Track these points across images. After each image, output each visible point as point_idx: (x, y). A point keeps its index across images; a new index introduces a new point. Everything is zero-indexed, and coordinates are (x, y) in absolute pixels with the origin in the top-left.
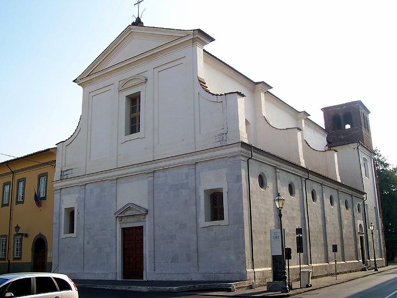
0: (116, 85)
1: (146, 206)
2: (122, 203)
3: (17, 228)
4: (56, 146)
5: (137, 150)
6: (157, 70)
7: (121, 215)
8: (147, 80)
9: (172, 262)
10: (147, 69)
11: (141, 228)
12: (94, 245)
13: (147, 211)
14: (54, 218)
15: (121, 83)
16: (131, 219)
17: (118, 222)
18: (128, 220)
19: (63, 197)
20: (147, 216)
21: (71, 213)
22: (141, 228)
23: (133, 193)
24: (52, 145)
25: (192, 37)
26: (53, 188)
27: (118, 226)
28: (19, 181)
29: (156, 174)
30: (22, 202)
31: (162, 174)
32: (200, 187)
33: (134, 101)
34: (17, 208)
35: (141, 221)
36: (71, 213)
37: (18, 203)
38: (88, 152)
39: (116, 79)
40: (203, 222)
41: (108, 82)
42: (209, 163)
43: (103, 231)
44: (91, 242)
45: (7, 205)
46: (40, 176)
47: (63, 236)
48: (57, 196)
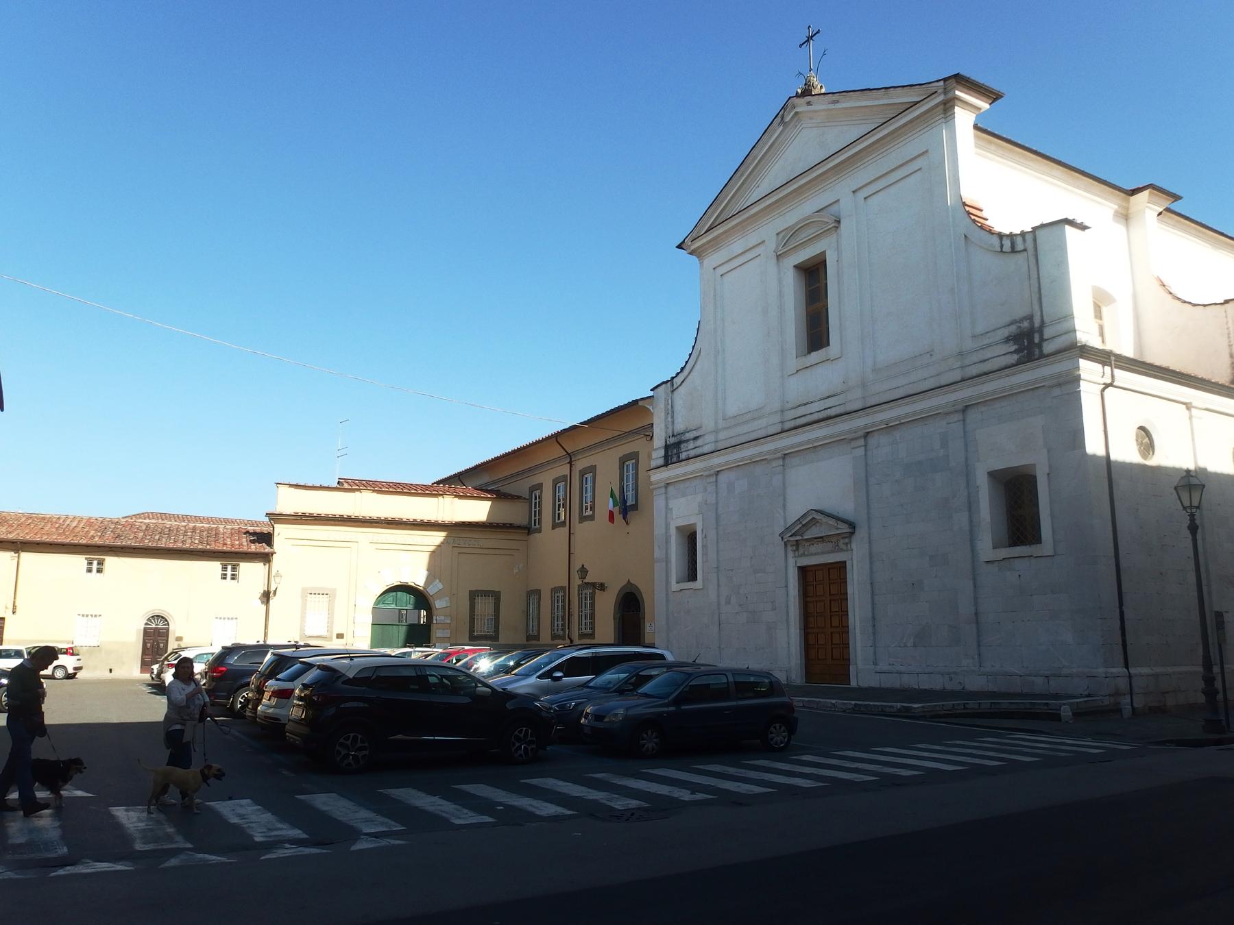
0: (771, 245)
1: (846, 507)
2: (796, 509)
3: (583, 571)
4: (651, 394)
5: (824, 378)
8: (839, 222)
9: (915, 646)
10: (840, 192)
11: (842, 566)
13: (852, 525)
14: (656, 548)
17: (791, 554)
18: (813, 549)
21: (690, 538)
22: (842, 566)
23: (821, 485)
25: (941, 98)
27: (791, 561)
28: (583, 473)
29: (872, 441)
31: (884, 439)
33: (813, 275)
34: (581, 529)
35: (842, 550)
36: (690, 538)
37: (583, 519)
39: (768, 232)
41: (752, 238)
44: (733, 600)
45: (564, 523)
46: (623, 461)
47: (674, 586)
48: (659, 502)
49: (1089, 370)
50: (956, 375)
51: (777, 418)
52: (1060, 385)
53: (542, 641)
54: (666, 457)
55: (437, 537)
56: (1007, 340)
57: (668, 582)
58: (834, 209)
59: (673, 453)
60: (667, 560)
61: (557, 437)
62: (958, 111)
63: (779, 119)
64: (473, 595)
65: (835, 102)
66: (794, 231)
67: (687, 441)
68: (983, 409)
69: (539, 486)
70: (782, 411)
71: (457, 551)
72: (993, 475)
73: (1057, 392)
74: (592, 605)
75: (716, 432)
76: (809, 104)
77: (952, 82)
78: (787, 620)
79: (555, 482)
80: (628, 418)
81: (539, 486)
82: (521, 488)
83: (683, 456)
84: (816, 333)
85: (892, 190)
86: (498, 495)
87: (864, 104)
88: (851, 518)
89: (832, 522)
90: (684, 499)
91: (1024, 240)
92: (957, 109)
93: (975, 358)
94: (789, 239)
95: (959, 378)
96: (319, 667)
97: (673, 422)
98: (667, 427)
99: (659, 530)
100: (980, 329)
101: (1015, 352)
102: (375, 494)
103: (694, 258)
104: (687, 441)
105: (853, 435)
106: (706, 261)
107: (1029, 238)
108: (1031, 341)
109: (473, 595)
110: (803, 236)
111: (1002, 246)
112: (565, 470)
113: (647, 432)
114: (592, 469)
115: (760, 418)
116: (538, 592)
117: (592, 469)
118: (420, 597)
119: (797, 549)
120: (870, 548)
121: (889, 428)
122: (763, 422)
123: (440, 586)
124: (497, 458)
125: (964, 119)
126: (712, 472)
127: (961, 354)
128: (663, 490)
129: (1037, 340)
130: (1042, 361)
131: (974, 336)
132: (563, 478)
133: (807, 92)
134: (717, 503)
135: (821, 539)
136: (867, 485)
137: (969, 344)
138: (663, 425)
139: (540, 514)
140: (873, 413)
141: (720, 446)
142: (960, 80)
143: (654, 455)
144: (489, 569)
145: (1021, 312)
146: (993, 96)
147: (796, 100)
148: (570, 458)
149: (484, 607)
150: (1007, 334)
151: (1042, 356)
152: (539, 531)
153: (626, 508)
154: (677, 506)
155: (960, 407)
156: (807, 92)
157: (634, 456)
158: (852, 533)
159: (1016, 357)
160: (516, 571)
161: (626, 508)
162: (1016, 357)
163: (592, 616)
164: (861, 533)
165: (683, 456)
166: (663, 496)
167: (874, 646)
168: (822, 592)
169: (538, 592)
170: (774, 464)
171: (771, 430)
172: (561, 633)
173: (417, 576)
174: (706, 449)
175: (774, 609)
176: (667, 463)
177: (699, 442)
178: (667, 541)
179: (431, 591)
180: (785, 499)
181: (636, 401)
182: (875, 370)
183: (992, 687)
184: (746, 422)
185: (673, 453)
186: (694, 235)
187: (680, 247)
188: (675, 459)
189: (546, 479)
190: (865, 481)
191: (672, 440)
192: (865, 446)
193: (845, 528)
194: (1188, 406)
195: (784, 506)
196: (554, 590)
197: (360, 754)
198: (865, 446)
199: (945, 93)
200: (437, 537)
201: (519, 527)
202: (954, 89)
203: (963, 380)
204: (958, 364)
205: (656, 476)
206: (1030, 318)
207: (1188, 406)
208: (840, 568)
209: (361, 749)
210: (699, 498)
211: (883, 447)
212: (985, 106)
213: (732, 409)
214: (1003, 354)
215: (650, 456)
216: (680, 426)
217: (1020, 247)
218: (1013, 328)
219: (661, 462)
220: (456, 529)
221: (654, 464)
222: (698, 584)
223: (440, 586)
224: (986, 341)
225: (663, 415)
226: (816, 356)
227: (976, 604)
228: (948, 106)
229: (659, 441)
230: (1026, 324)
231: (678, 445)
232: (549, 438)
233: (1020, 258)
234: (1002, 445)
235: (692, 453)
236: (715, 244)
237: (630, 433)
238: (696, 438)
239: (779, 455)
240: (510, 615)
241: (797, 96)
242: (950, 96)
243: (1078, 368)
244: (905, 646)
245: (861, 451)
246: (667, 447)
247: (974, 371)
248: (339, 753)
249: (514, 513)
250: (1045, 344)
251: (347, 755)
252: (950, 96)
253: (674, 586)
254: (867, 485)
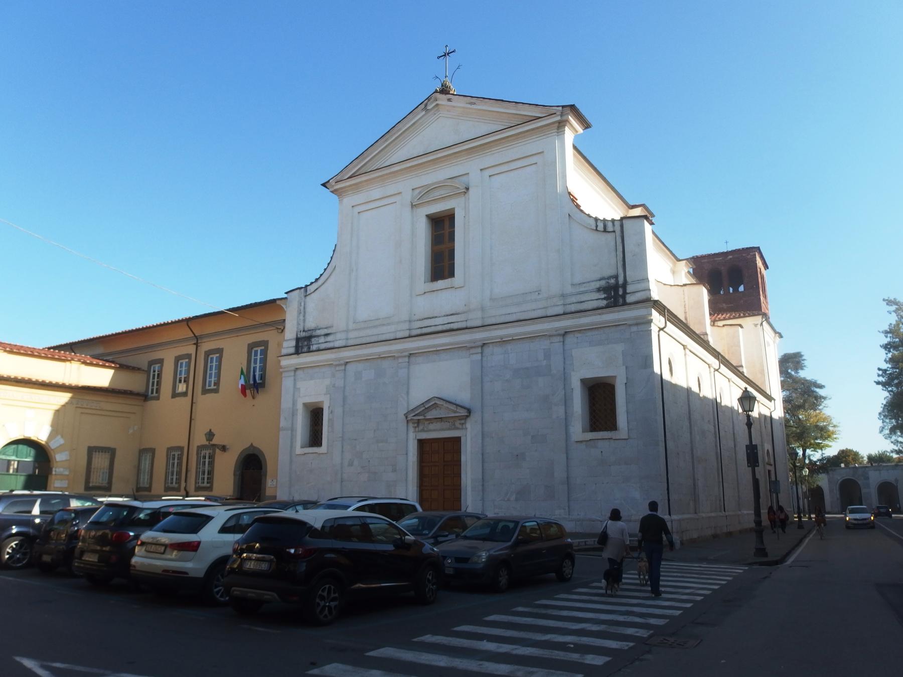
0: (408, 197)
1: (464, 397)
2: (419, 395)
3: (210, 435)
4: (286, 296)
5: (445, 300)
6: (487, 173)
7: (418, 416)
8: (467, 189)
9: (517, 500)
10: (471, 168)
11: (458, 440)
12: (362, 467)
13: (469, 411)
14: (282, 419)
15: (417, 191)
16: (438, 425)
17: (411, 430)
18: (431, 426)
19: (300, 384)
20: (469, 420)
21: (315, 415)
22: (458, 440)
23: (442, 378)
24: (277, 293)
25: (558, 118)
26: (281, 367)
27: (412, 435)
28: (208, 354)
29: (487, 350)
30: (216, 391)
31: (497, 350)
32: (573, 373)
33: (442, 226)
34: (205, 402)
35: (458, 429)
36: (315, 415)
37: (205, 391)
38: (103, 413)
39: (406, 186)
40: (577, 428)
41: (391, 189)
42: (589, 333)
43: (380, 445)
44: (356, 463)
45: (185, 394)
46: (251, 347)
47: (299, 450)
48: (287, 383)
49: (657, 319)
50: (560, 310)
51: (406, 326)
52: (637, 324)
53: (153, 492)
54: (297, 347)
55: (64, 397)
56: (599, 290)
57: (292, 446)
58: (464, 179)
59: (303, 344)
60: (293, 429)
61: (188, 321)
62: (567, 129)
63: (423, 106)
64: (91, 451)
65: (471, 103)
66: (428, 190)
67: (318, 336)
68: (579, 335)
69: (161, 361)
70: (410, 321)
71: (80, 410)
72: (584, 381)
73: (634, 329)
74: (212, 464)
75: (347, 331)
76: (449, 100)
77: (568, 110)
78: (406, 480)
79: (178, 359)
80: (264, 313)
81: (161, 361)
82: (142, 360)
83: (314, 347)
84: (442, 265)
85: (512, 174)
86: (121, 367)
87: (484, 108)
88: (467, 405)
89: (453, 407)
90: (312, 382)
91: (614, 225)
92: (566, 128)
93: (574, 299)
94: (424, 195)
95: (562, 312)
96: (176, 514)
97: (304, 321)
98: (298, 324)
99: (286, 403)
100: (577, 280)
101: (604, 299)
102: (6, 354)
103: (334, 197)
104: (318, 336)
105: (473, 345)
106: (346, 200)
107: (617, 225)
108: (616, 291)
109: (91, 451)
110: (437, 194)
111: (597, 226)
112: (191, 350)
113: (280, 326)
114: (220, 351)
115: (389, 324)
116: (153, 451)
117: (220, 351)
118: (41, 451)
119: (418, 426)
120: (482, 428)
121: (503, 342)
122: (392, 328)
123: (62, 441)
124: (117, 334)
125: (569, 136)
126: (342, 362)
127: (563, 296)
128: (292, 374)
129: (621, 292)
130: (626, 307)
131: (572, 285)
132: (188, 356)
133: (444, 90)
134: (344, 387)
135: (441, 419)
136: (482, 382)
137: (569, 289)
138: (295, 322)
139: (159, 383)
140: (490, 330)
141: (351, 342)
142: (573, 108)
143: (285, 344)
144: (106, 429)
145: (610, 272)
146: (586, 125)
147: (438, 95)
148: (197, 341)
149: (101, 461)
150: (598, 286)
151: (625, 303)
152: (158, 398)
153: (255, 385)
154: (303, 385)
155: (562, 332)
156: (444, 90)
157: (265, 344)
158: (467, 416)
159: (605, 302)
160: (131, 431)
161: (255, 385)
162: (605, 302)
163: (211, 473)
164: (476, 417)
165: (314, 347)
166: (292, 378)
167: (483, 499)
168: (439, 461)
169: (153, 451)
170: (400, 360)
171: (399, 335)
172: (177, 486)
173: (42, 434)
174: (337, 344)
175: (394, 471)
176: (298, 351)
177: (329, 338)
178: (294, 414)
179: (53, 445)
180: (408, 389)
181: (274, 301)
182: (492, 299)
183: (579, 530)
184: (375, 327)
185: (303, 344)
186: (339, 178)
187: (324, 185)
188: (305, 349)
189: (168, 356)
190: (480, 379)
191: (303, 334)
192: (482, 353)
193: (463, 413)
194: (685, 347)
195: (408, 393)
196: (170, 450)
197: (333, 604)
198: (482, 353)
199: (561, 116)
200: (64, 397)
201: (138, 394)
202: (568, 114)
203: (564, 314)
204: (561, 302)
205: (285, 362)
206: (616, 277)
207: (685, 347)
208: (456, 442)
209: (333, 600)
210: (327, 382)
211: (496, 356)
212: (580, 130)
213: (363, 314)
214: (596, 299)
215: (280, 345)
216: (310, 324)
217: (610, 228)
218: (603, 283)
219: (292, 350)
220: (80, 391)
221: (284, 351)
222: (323, 449)
223: (62, 441)
224: (582, 289)
225: (295, 313)
226: (441, 284)
227: (568, 471)
228: (561, 125)
229: (291, 332)
230: (613, 281)
231: (309, 338)
232: (183, 320)
233: (610, 236)
234: (592, 361)
235: (323, 346)
236: (356, 188)
237: (266, 324)
238: (327, 335)
239: (407, 354)
240: (124, 466)
241: (436, 91)
242: (564, 118)
243: (651, 315)
244: (508, 500)
245: (479, 357)
246: (298, 340)
247: (573, 308)
248: (319, 604)
249: (134, 382)
250: (628, 296)
251: (324, 607)
252: (564, 118)
253: (299, 450)
254: (482, 382)
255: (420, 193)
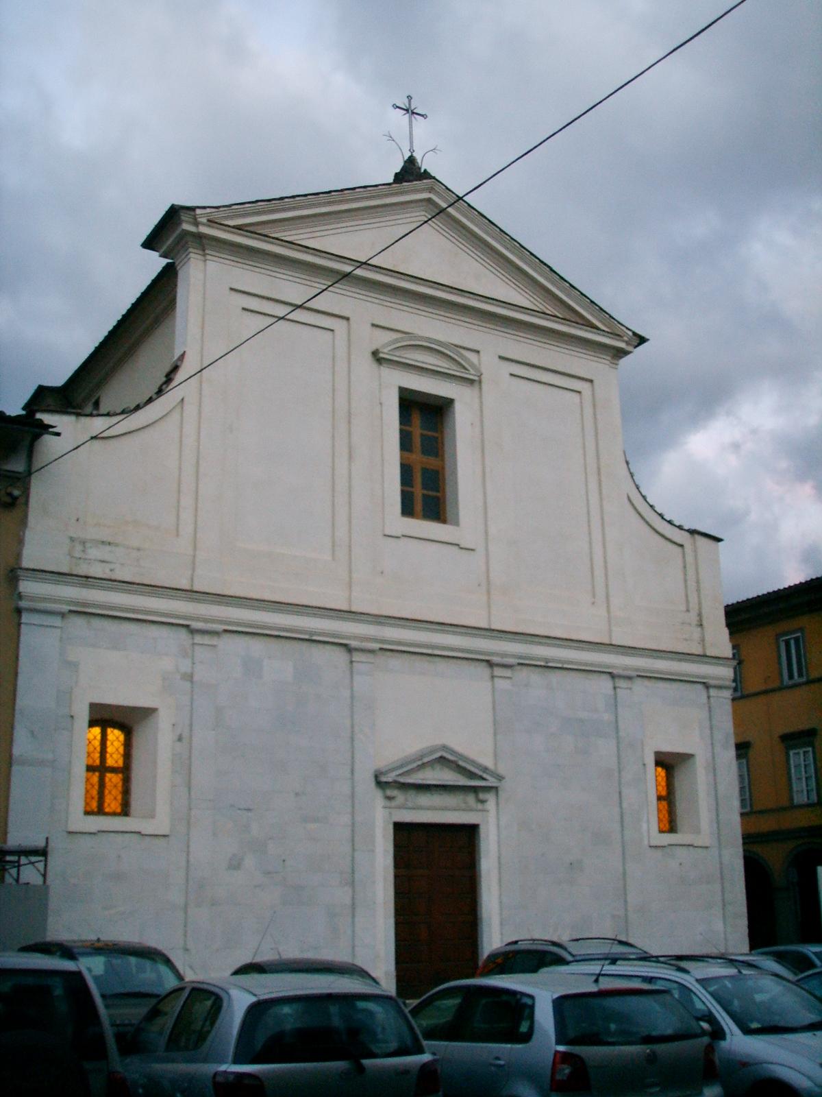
11: (471, 831)
22: (471, 831)
42: (661, 684)
255: (396, 341)
